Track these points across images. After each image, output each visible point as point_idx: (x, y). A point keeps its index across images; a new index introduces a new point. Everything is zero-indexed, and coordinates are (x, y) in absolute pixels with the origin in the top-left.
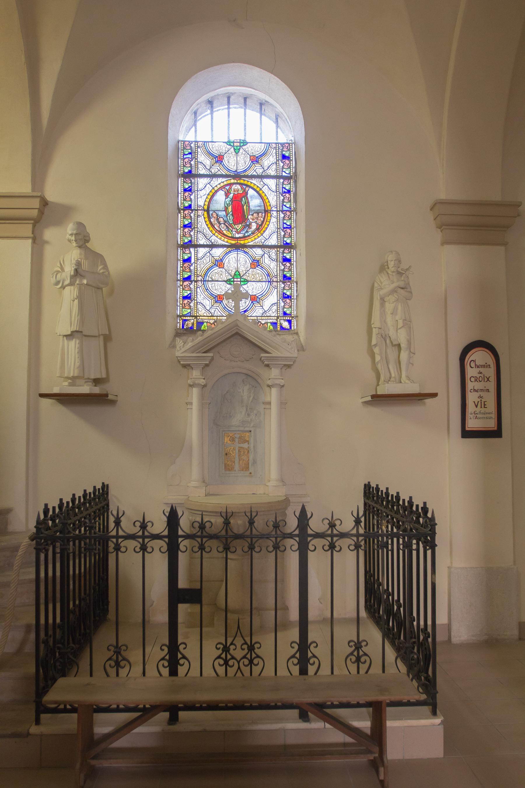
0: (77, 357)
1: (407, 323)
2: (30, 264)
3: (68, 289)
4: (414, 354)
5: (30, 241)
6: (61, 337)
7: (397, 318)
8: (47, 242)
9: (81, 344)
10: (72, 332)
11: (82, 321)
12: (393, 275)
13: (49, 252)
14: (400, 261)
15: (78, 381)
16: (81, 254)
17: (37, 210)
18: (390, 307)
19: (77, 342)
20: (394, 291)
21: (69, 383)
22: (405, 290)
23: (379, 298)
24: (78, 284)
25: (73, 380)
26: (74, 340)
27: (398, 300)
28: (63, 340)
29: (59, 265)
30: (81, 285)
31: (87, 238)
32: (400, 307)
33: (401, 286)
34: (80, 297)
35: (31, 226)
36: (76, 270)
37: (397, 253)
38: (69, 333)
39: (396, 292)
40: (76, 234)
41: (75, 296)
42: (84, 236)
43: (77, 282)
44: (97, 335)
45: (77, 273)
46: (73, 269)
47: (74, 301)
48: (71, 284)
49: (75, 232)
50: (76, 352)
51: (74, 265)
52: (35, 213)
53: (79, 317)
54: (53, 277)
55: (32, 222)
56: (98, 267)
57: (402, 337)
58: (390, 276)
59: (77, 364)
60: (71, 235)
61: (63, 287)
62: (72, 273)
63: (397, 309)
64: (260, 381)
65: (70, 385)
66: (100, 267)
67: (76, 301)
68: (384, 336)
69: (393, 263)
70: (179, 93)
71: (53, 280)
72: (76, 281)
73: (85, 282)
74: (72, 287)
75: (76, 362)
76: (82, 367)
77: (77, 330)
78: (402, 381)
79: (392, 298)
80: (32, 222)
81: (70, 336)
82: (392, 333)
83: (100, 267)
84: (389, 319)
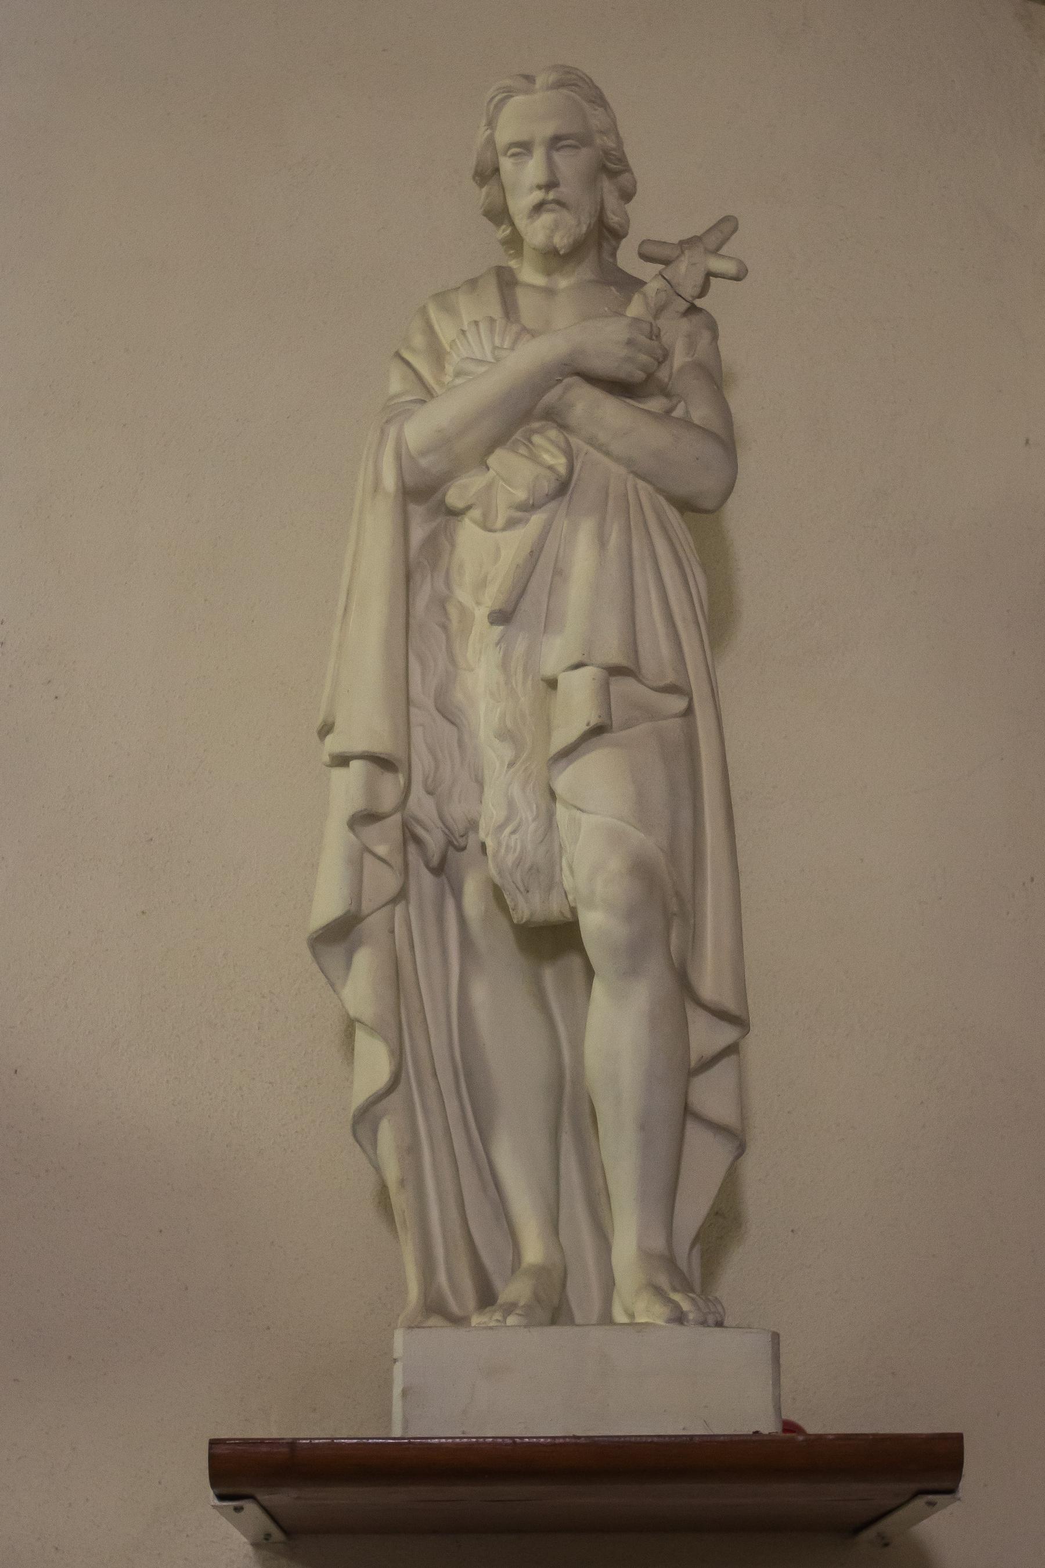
1: (660, 710)
4: (739, 1021)
7: (555, 653)
12: (550, 292)
14: (611, 167)
18: (483, 557)
20: (527, 411)
22: (656, 404)
23: (389, 481)
27: (563, 488)
32: (583, 556)
33: (600, 365)
37: (577, 85)
39: (555, 417)
57: (590, 845)
58: (525, 301)
63: (559, 573)
68: (434, 842)
69: (534, 169)
70: (700, 1224)
78: (620, 1317)
79: (516, 473)
82: (499, 806)
84: (483, 676)
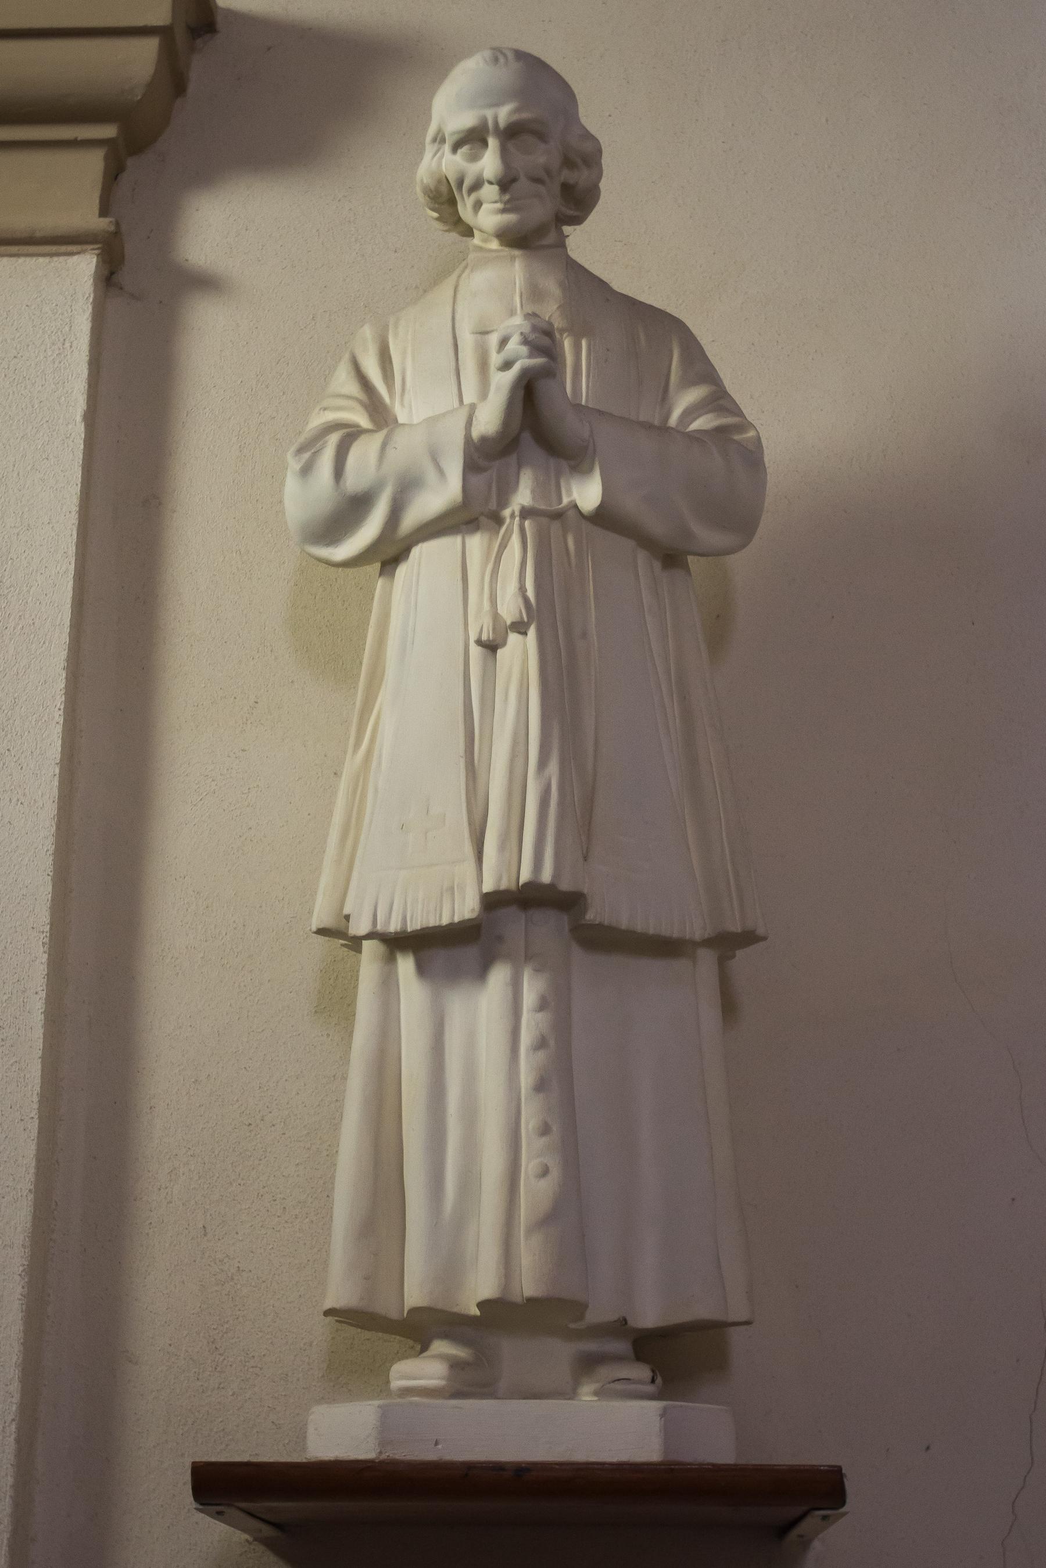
0: (529, 1122)
2: (79, 430)
3: (431, 559)
5: (84, 266)
6: (370, 958)
8: (204, 283)
9: (558, 1004)
10: (492, 902)
11: (579, 813)
13: (215, 347)
15: (513, 1353)
16: (534, 293)
17: (151, 46)
19: (529, 997)
21: (456, 1365)
24: (526, 513)
25: (487, 1337)
26: (499, 976)
28: (388, 984)
29: (353, 388)
30: (551, 518)
31: (581, 177)
34: (551, 613)
35: (94, 162)
36: (529, 396)
38: (465, 907)
40: (511, 134)
41: (510, 608)
42: (568, 163)
43: (523, 496)
44: (696, 929)
45: (534, 426)
46: (503, 382)
47: (491, 647)
48: (466, 518)
49: (504, 114)
50: (526, 1079)
51: (514, 345)
52: (140, 58)
53: (553, 768)
54: (307, 470)
55: (108, 131)
56: (664, 399)
59: (536, 1192)
60: (473, 139)
61: (389, 554)
62: (488, 419)
64: (267, 1531)
65: (472, 1381)
66: (685, 399)
67: (521, 653)
71: (305, 496)
72: (505, 491)
73: (587, 493)
74: (476, 543)
75: (529, 1166)
76: (569, 1219)
77: (546, 876)
80: (108, 131)
81: (445, 950)
83: (685, 399)
